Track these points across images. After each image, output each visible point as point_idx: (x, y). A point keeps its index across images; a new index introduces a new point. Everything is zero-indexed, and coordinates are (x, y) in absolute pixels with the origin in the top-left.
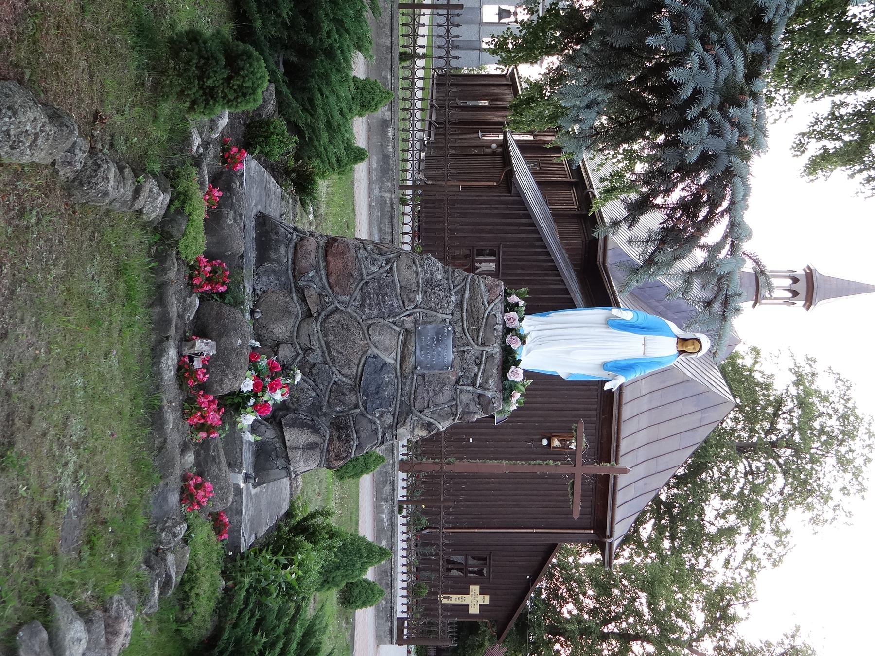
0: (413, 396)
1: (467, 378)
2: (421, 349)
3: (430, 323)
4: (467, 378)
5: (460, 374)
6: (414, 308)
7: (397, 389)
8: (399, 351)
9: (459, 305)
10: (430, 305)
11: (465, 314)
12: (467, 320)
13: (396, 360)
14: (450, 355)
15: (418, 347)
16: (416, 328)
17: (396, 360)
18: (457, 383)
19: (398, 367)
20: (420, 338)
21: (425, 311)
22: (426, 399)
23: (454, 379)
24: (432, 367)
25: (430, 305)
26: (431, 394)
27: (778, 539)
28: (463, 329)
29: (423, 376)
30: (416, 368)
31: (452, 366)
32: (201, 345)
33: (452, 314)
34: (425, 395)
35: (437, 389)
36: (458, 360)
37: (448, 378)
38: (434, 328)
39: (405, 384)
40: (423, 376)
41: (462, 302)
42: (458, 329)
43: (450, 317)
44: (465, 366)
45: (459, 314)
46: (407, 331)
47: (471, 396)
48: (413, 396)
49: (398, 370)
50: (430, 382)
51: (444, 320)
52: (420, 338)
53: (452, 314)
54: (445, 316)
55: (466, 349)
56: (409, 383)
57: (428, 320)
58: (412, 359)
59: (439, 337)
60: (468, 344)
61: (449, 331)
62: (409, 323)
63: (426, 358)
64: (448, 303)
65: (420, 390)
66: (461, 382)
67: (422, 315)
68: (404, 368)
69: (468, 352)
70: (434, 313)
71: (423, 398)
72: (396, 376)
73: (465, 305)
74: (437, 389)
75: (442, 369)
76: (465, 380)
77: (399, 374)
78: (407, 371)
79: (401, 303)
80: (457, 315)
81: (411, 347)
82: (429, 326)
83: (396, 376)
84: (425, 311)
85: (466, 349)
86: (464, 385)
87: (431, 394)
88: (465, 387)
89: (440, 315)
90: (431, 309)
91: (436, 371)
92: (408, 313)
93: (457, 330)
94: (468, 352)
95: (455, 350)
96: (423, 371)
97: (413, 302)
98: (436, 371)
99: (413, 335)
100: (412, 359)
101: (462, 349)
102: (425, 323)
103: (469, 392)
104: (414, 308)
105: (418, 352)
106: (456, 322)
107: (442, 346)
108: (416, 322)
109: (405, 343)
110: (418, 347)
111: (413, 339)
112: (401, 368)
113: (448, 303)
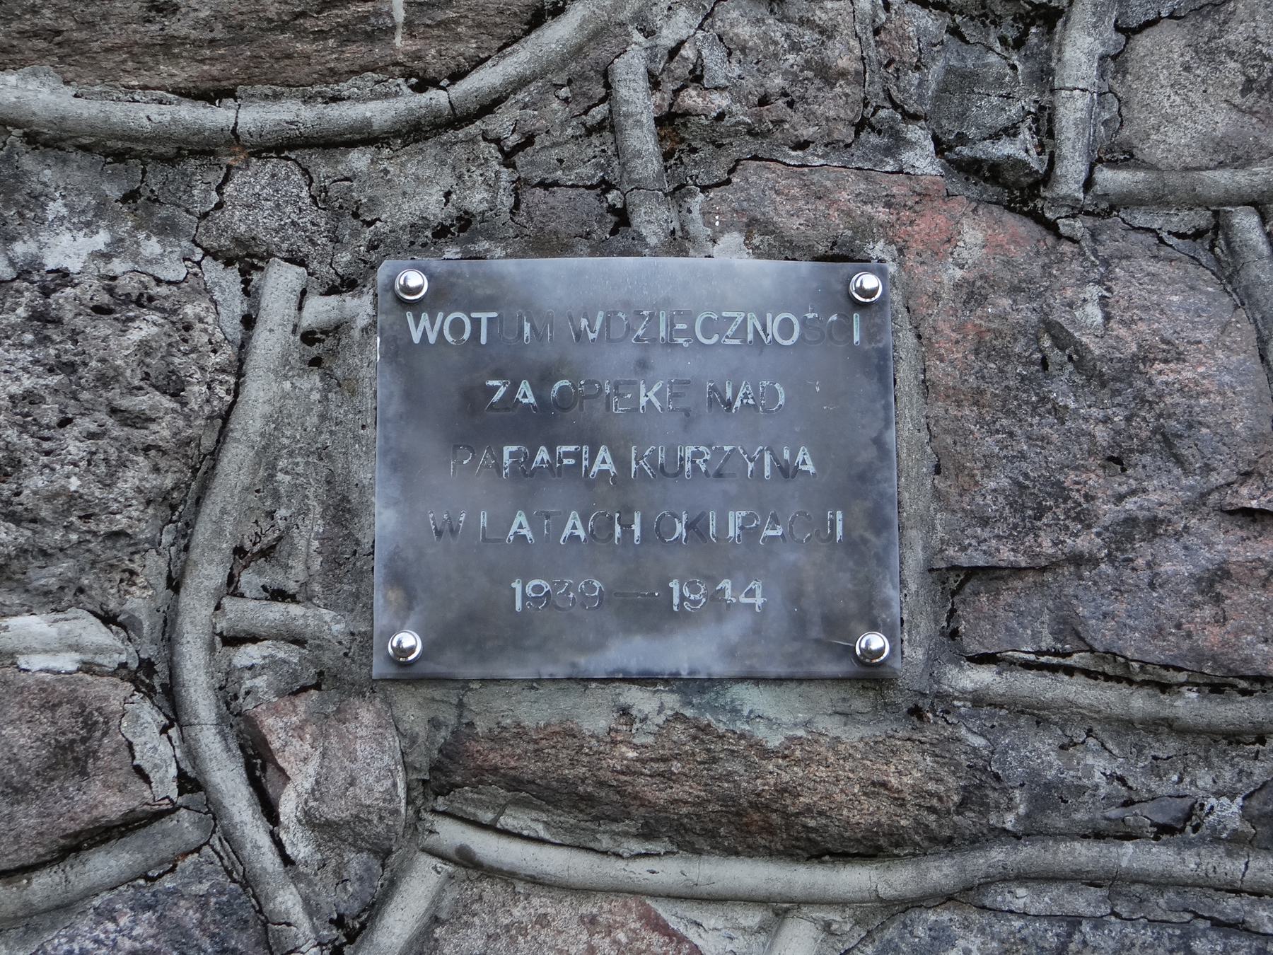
0: (1188, 705)
1: (961, 83)
2: (653, 613)
3: (343, 511)
4: (961, 83)
5: (922, 160)
6: (174, 713)
7: (1110, 882)
8: (671, 871)
9: (142, 173)
10: (134, 518)
11: (254, 116)
12: (324, 84)
13: (780, 908)
14: (713, 288)
15: (630, 652)
16: (407, 674)
17: (780, 908)
18: (1021, 192)
19: (855, 879)
20: (518, 633)
21: (208, 573)
22: (1230, 546)
23: (981, 236)
24: (858, 479)
25: (134, 518)
26: (1160, 492)
27: (134, 298)
28: (413, 132)
29: (956, 582)
30: (871, 677)
31: (843, 254)
32: (610, 197)
33: (247, 260)
34: (1176, 565)
35: (1097, 419)
36: (769, 188)
37: (972, 294)
38: (402, 464)
39: (1049, 796)
40: (956, 582)
41: (116, 150)
42: (420, 189)
43: (281, 280)
44: (834, 106)
45: (254, 180)
46: (443, 778)
47: (1164, 48)
48: (1188, 705)
49: (896, 879)
50: (1032, 503)
51: (319, 347)
52: (518, 633)
53: (247, 260)
54: (271, 341)
55: (638, 102)
56: (1041, 752)
57: (309, 536)
58: (772, 716)
59: (510, 408)
60: (589, 77)
61: (441, 295)
62: (351, 761)
63: (751, 554)
64: (116, 304)
65: (1118, 623)
66: (1022, 147)
67: (251, 611)
68: (866, 813)
69: (674, 72)
70: (236, 464)
71: (1213, 582)
72: (965, 896)
73: (146, 114)
74: (1097, 419)
75: (879, 366)
76: (987, 109)
77: (941, 872)
78: (910, 770)
79: (104, 864)
80: (260, 199)
81: (621, 728)
82: (384, 521)
83: (965, 896)
84: (208, 573)
85: (638, 102)
86: (1045, 124)
87: (1160, 492)
88: (1072, 113)
89: (260, 392)
90: (179, 509)
91: (905, 432)
92: (228, 779)
93: (431, 204)
94: (674, 72)
95: (651, 220)
96: (904, 588)
97: (92, 722)
98: (905, 432)
99: (492, 709)
100: (772, 716)
101: (642, 140)
102: (345, 563)
103: (1114, 62)
104: (174, 713)
105: (689, 652)
106: (344, 210)
107: (613, 363)
108: (330, 681)
109: (586, 804)
110: (630, 652)
111: (534, 713)
112: (870, 848)
113: (116, 304)
